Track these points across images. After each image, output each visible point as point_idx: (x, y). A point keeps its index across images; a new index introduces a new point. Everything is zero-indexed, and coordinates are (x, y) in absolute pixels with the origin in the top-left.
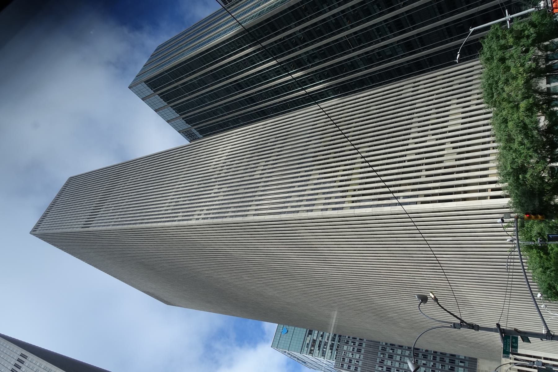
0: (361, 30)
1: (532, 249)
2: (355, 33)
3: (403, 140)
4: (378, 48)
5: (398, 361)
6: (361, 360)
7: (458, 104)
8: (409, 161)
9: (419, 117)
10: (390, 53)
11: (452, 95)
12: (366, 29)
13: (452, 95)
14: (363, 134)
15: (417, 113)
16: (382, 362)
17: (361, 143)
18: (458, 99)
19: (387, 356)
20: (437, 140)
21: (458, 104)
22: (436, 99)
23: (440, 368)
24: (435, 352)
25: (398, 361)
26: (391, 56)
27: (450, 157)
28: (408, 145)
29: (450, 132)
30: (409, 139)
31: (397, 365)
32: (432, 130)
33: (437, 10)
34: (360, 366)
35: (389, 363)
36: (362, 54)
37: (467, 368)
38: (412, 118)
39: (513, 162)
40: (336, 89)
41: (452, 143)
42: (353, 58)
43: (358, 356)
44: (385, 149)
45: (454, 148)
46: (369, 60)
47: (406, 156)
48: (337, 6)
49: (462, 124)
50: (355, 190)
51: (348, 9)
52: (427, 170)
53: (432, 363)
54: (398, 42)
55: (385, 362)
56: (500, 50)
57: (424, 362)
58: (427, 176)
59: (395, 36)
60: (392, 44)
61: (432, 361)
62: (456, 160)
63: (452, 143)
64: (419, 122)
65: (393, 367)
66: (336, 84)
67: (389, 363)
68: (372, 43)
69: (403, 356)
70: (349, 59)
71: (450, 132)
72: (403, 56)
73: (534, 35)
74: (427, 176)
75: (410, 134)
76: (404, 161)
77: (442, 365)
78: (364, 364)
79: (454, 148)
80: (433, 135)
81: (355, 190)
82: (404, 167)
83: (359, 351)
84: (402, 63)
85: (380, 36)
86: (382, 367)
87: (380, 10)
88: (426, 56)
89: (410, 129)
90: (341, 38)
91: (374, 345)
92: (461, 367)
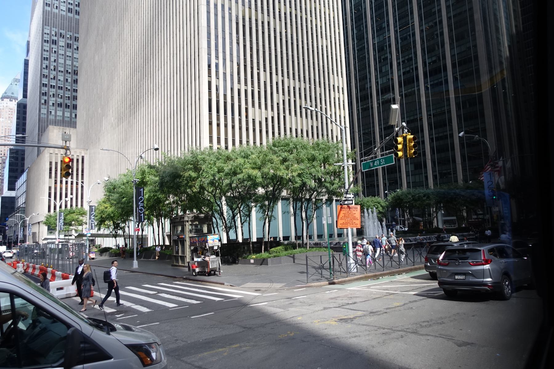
0: (414, 42)
1: (142, 175)
2: (414, 34)
3: (282, 70)
4: (391, 59)
5: (65, 53)
7: (312, 127)
8: (258, 74)
9: (305, 89)
10: (384, 71)
11: (322, 123)
12: (415, 46)
13: (322, 123)
14: (297, 28)
15: (310, 87)
17: (286, 23)
18: (317, 127)
19: (69, 42)
20: (278, 104)
21: (312, 127)
25: (65, 53)
26: (381, 71)
27: (257, 114)
28: (277, 74)
29: (284, 117)
30: (283, 76)
32: (289, 100)
33: (412, 118)
34: (51, 9)
35: (62, 42)
36: (390, 41)
37: (71, 120)
38: (305, 82)
39: (204, 160)
40: (360, 8)
41: (273, 118)
42: (389, 30)
43: (64, 9)
44: (276, 50)
45: (266, 119)
46: (382, 49)
47: (265, 71)
48: (449, 15)
49: (291, 129)
50: (230, 9)
51: (442, 28)
52: (246, 91)
53: (69, 88)
54: (392, 79)
55: (61, 39)
56: (324, 157)
57: (69, 80)
59: (399, 77)
60: (392, 73)
61: (71, 88)
62: (253, 119)
63: (273, 118)
64: (300, 89)
65: (58, 48)
66: (365, 9)
67: (62, 42)
68: (398, 53)
69: (72, 59)
70: (388, 25)
71: (284, 117)
72: (377, 83)
74: (239, 91)
75: (288, 78)
76: (258, 69)
77: (69, 97)
78: (55, 15)
79: (266, 119)
80: (284, 101)
81: (230, 9)
82: (252, 68)
83: (70, 10)
84: (370, 81)
85: (403, 62)
86: (56, 36)
87: (429, 63)
88: (372, 105)
89: (294, 79)
90: (412, 18)
91: (75, 27)
92: (71, 115)
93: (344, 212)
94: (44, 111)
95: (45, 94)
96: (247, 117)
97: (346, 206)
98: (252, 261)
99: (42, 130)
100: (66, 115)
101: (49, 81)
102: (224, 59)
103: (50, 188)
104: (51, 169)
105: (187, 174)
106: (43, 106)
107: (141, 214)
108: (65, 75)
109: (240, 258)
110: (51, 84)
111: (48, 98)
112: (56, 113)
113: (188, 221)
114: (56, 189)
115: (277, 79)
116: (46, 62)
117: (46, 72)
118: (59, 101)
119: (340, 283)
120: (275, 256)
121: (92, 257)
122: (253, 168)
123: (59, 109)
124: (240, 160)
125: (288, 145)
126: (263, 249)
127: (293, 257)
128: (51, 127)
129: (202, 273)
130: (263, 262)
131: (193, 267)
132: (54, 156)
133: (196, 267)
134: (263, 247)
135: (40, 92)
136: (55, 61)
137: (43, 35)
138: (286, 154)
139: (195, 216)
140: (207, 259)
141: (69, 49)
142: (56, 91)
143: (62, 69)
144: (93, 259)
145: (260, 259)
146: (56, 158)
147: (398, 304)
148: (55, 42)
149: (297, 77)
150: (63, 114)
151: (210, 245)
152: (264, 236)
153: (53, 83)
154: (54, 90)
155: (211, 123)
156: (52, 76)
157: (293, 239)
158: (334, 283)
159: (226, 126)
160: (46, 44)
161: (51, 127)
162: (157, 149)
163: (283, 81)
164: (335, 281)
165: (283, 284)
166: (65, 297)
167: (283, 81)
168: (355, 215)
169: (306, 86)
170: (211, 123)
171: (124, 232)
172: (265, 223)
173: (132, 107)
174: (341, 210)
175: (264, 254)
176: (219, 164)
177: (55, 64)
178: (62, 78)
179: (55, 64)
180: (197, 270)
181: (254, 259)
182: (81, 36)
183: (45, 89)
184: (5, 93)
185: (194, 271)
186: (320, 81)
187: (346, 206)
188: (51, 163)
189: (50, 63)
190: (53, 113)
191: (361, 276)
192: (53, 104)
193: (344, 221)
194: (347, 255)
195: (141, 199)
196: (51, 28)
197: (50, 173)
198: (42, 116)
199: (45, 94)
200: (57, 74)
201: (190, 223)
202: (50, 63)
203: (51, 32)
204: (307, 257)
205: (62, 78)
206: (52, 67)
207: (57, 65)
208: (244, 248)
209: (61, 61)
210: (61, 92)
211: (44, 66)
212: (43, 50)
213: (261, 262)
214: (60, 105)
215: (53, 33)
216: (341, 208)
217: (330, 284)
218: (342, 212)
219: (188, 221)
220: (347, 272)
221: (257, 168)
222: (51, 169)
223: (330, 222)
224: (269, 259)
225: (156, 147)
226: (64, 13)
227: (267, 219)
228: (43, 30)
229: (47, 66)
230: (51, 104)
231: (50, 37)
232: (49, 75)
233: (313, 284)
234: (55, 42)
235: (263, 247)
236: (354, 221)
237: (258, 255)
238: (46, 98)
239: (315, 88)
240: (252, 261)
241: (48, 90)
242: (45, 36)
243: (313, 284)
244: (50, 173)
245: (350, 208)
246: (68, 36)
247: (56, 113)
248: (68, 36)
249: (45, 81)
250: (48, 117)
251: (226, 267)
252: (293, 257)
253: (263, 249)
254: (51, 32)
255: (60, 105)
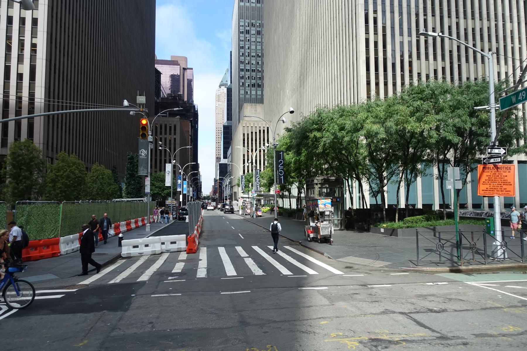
5: (256, 40)
6: (250, 5)
15: (496, 25)
16: (253, 25)
19: (258, 29)
20: (451, 52)
22: (513, 48)
23: (258, 76)
24: (262, 72)
25: (256, 40)
31: (253, 39)
34: (245, 4)
35: (253, 32)
37: (256, 96)
41: (444, 69)
55: (253, 28)
58: (402, 43)
63: (444, 69)
65: (250, 36)
67: (253, 32)
73: (191, 189)
74: (402, 43)
76: (425, 15)
78: (247, 8)
93: (489, 174)
94: (242, 92)
95: (242, 78)
96: (411, 71)
97: (491, 166)
98: (382, 230)
99: (240, 108)
100: (258, 94)
101: (245, 66)
102: (384, 12)
103: (244, 155)
104: (244, 140)
105: (312, 135)
106: (241, 88)
107: (281, 176)
108: (256, 59)
109: (372, 226)
110: (246, 68)
111: (245, 81)
112: (251, 92)
113: (317, 184)
114: (248, 156)
115: (450, 22)
116: (242, 50)
117: (242, 58)
118: (253, 82)
119: (469, 272)
120: (408, 227)
121: (260, 215)
122: (374, 123)
123: (253, 89)
124: (362, 115)
125: (422, 91)
126: (397, 218)
127: (434, 230)
128: (245, 105)
129: (314, 240)
130: (393, 232)
131: (308, 232)
132: (246, 128)
133: (312, 233)
134: (397, 215)
135: (239, 76)
136: (248, 48)
137: (239, 28)
138: (418, 103)
139: (324, 179)
140: (318, 225)
141: (259, 36)
142: (251, 74)
143: (254, 54)
144: (261, 216)
145: (390, 229)
146: (248, 131)
147: (512, 329)
148: (248, 32)
149: (477, 15)
150: (256, 92)
151: (321, 210)
152: (398, 202)
153: (248, 67)
154: (254, 73)
155: (368, 83)
156: (247, 62)
157: (437, 207)
158: (458, 271)
159: (386, 84)
160: (241, 35)
161: (245, 105)
162: (292, 112)
163: (458, 24)
164: (463, 268)
165: (387, 263)
166: (176, 250)
167: (458, 24)
168: (506, 178)
169: (482, 24)
170: (368, 83)
171: (290, 193)
172: (399, 188)
173: (302, 77)
174: (483, 171)
175: (397, 224)
176: (341, 121)
177: (249, 51)
178: (254, 62)
179: (249, 51)
180: (312, 235)
181: (385, 229)
182: (265, 22)
183: (242, 73)
184: (222, 82)
185: (309, 236)
186: (503, 15)
187: (491, 166)
188: (244, 135)
189: (245, 51)
190: (249, 93)
191: (510, 265)
192: (249, 85)
193: (488, 186)
194: (489, 231)
195: (281, 162)
196: (245, 21)
197: (244, 143)
198: (241, 96)
199: (242, 78)
200: (250, 59)
201: (319, 186)
202: (245, 51)
203: (245, 24)
204: (417, 233)
205: (254, 62)
206: (247, 54)
207: (250, 51)
208: (377, 215)
209: (253, 47)
210: (254, 74)
211: (241, 54)
212: (240, 40)
213: (390, 232)
214: (253, 85)
215: (247, 24)
216: (484, 168)
217: (452, 271)
218: (485, 174)
219: (317, 184)
220: (486, 254)
221: (379, 123)
222: (244, 140)
223: (459, 186)
224: (399, 230)
225: (292, 109)
226: (254, 5)
227: (403, 184)
228: (239, 23)
229: (243, 54)
230: (247, 85)
231: (245, 28)
232: (245, 61)
233: (424, 269)
234: (248, 32)
235: (397, 215)
236: (505, 187)
237: (389, 224)
238: (243, 81)
239: (504, 25)
240: (382, 230)
241: (245, 73)
242: (241, 28)
243: (424, 269)
244: (244, 143)
245: (497, 168)
246: (258, 24)
247: (251, 92)
248: (258, 24)
249: (242, 66)
250: (245, 96)
251: (352, 235)
252: (434, 230)
253: (397, 218)
254: (245, 24)
255: (253, 85)
